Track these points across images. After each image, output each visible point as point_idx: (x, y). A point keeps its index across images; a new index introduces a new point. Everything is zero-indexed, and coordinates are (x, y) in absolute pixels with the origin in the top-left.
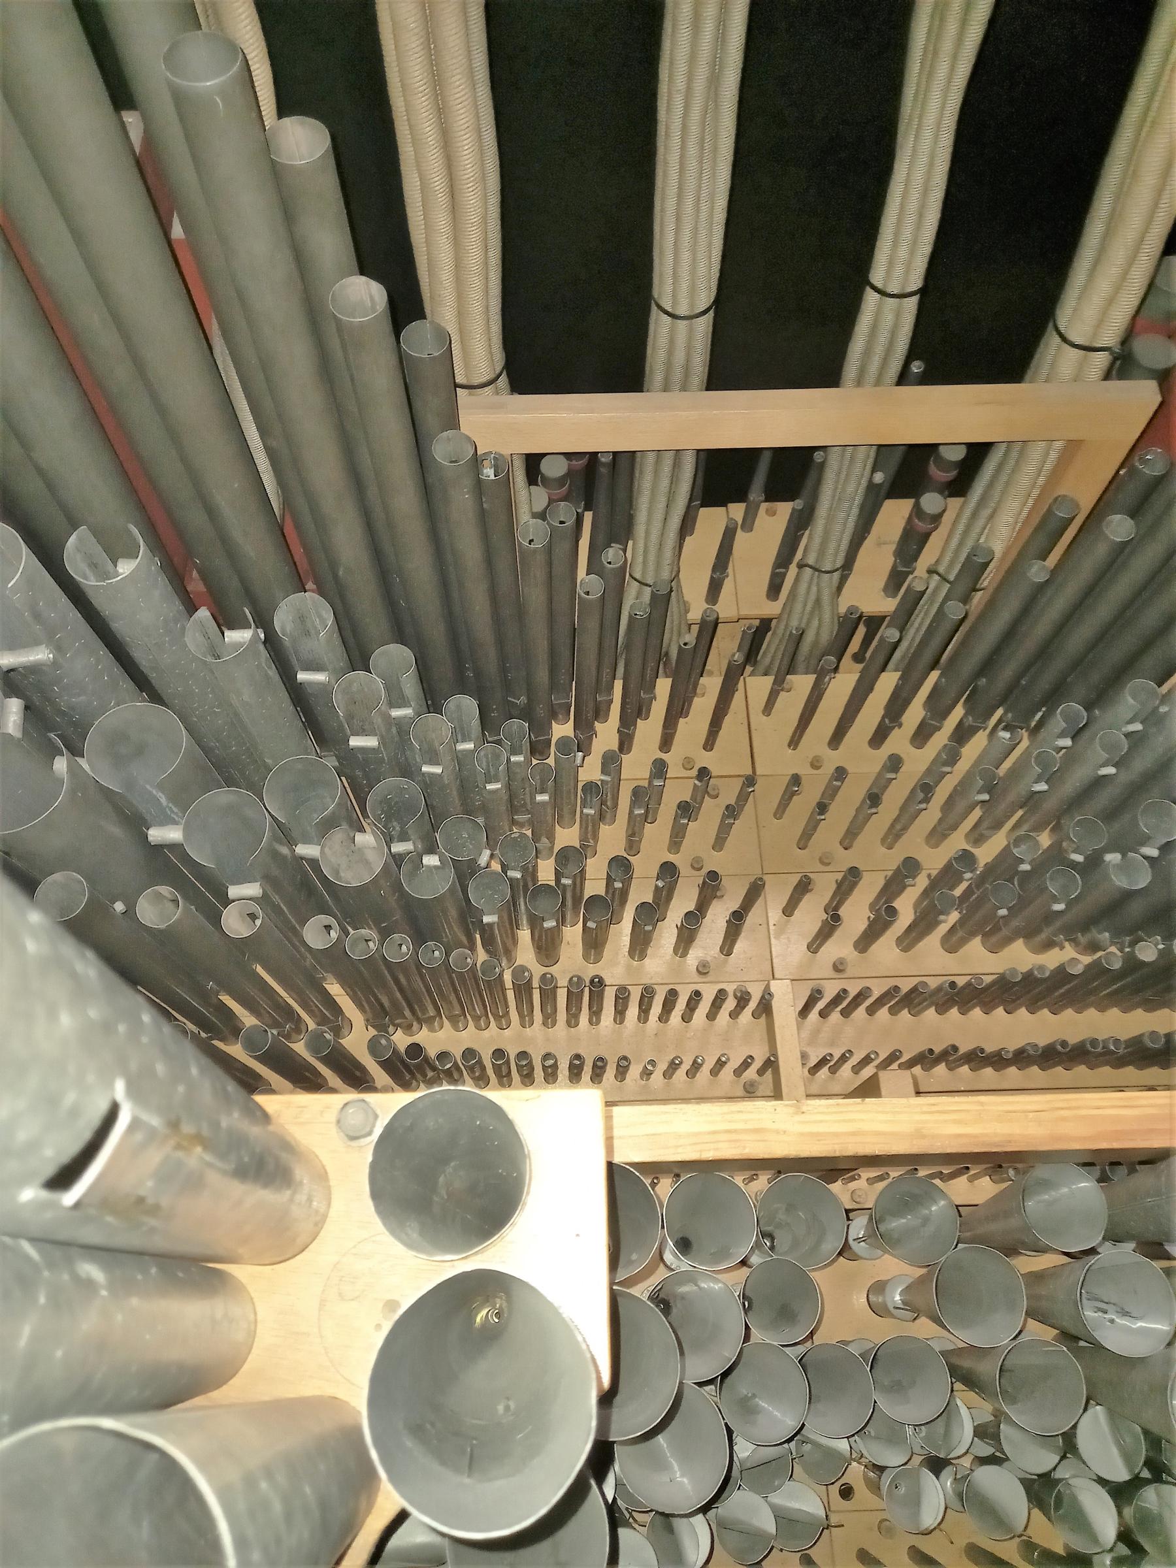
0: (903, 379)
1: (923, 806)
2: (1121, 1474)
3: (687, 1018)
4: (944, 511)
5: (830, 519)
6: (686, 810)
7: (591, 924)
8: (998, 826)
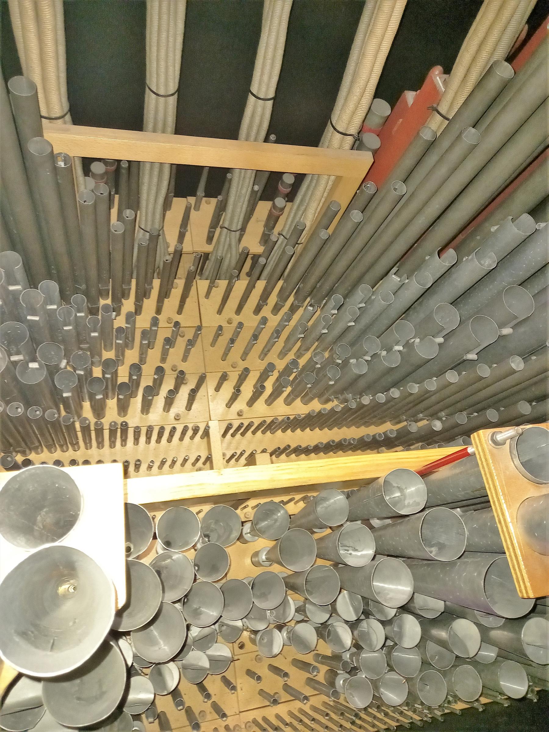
0: (266, 140)
1: (277, 340)
2: (353, 617)
3: (169, 440)
5: (235, 205)
6: (169, 342)
7: (121, 397)
8: (307, 349)
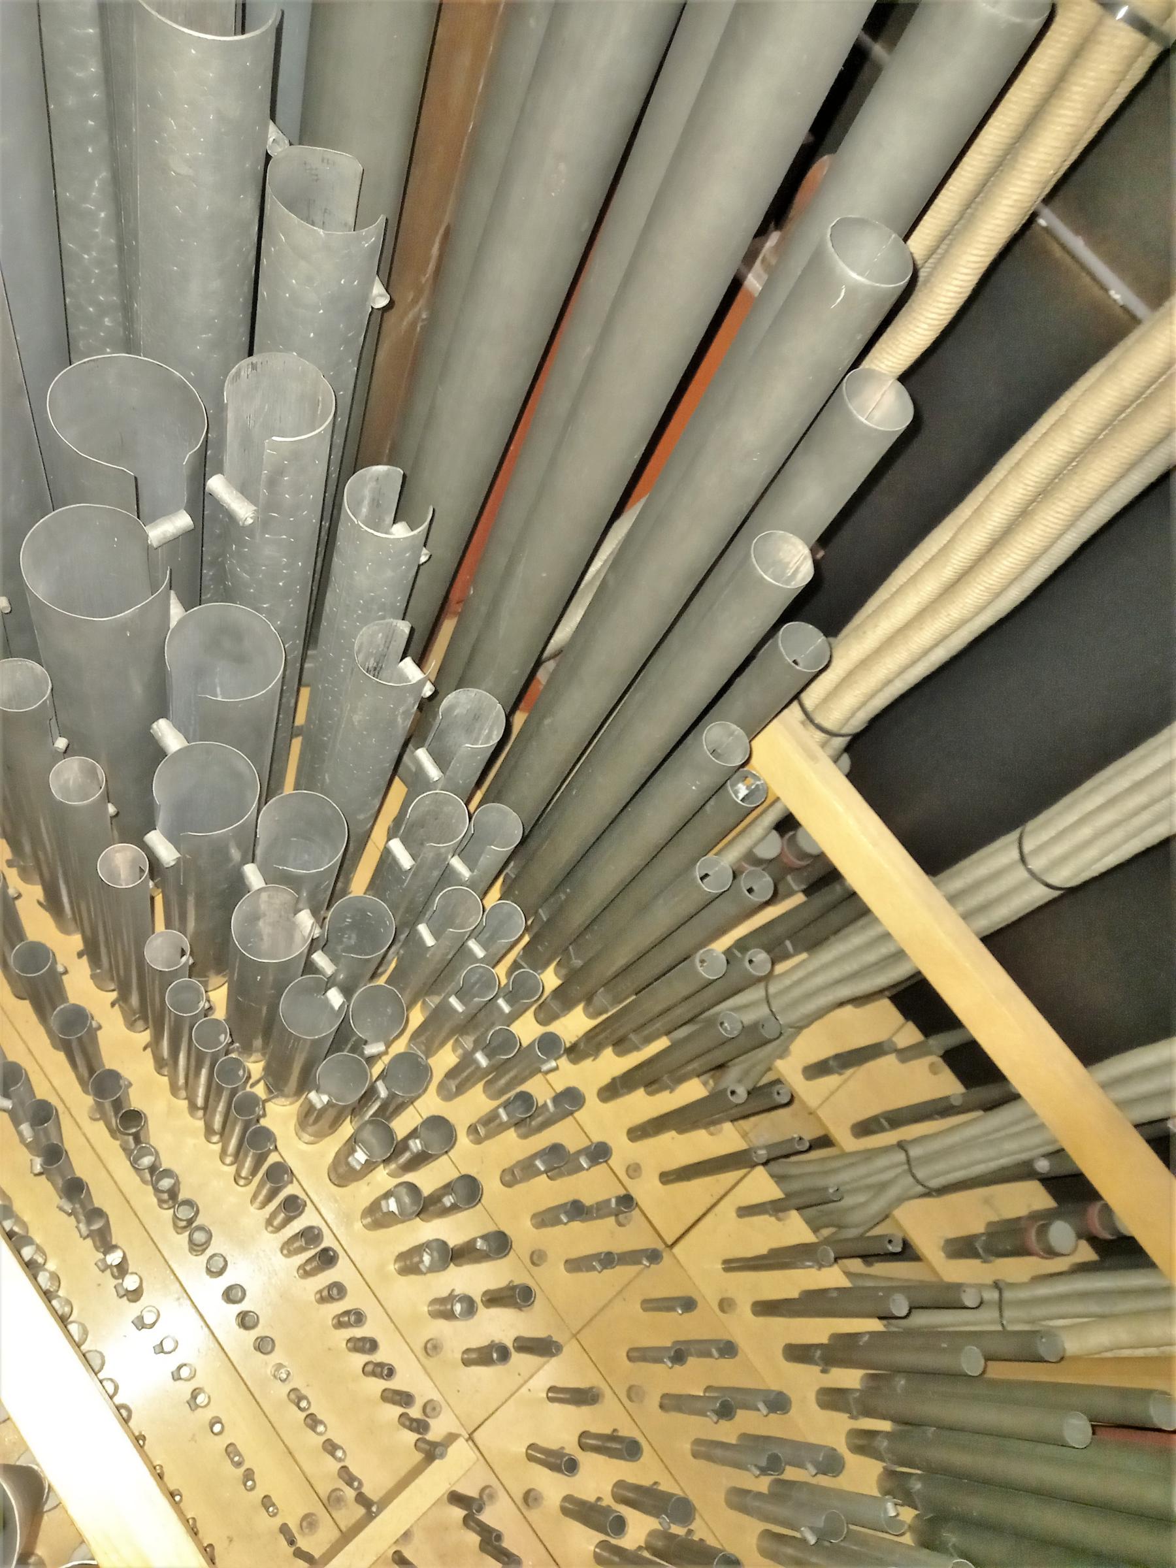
4: (1063, 1255)
